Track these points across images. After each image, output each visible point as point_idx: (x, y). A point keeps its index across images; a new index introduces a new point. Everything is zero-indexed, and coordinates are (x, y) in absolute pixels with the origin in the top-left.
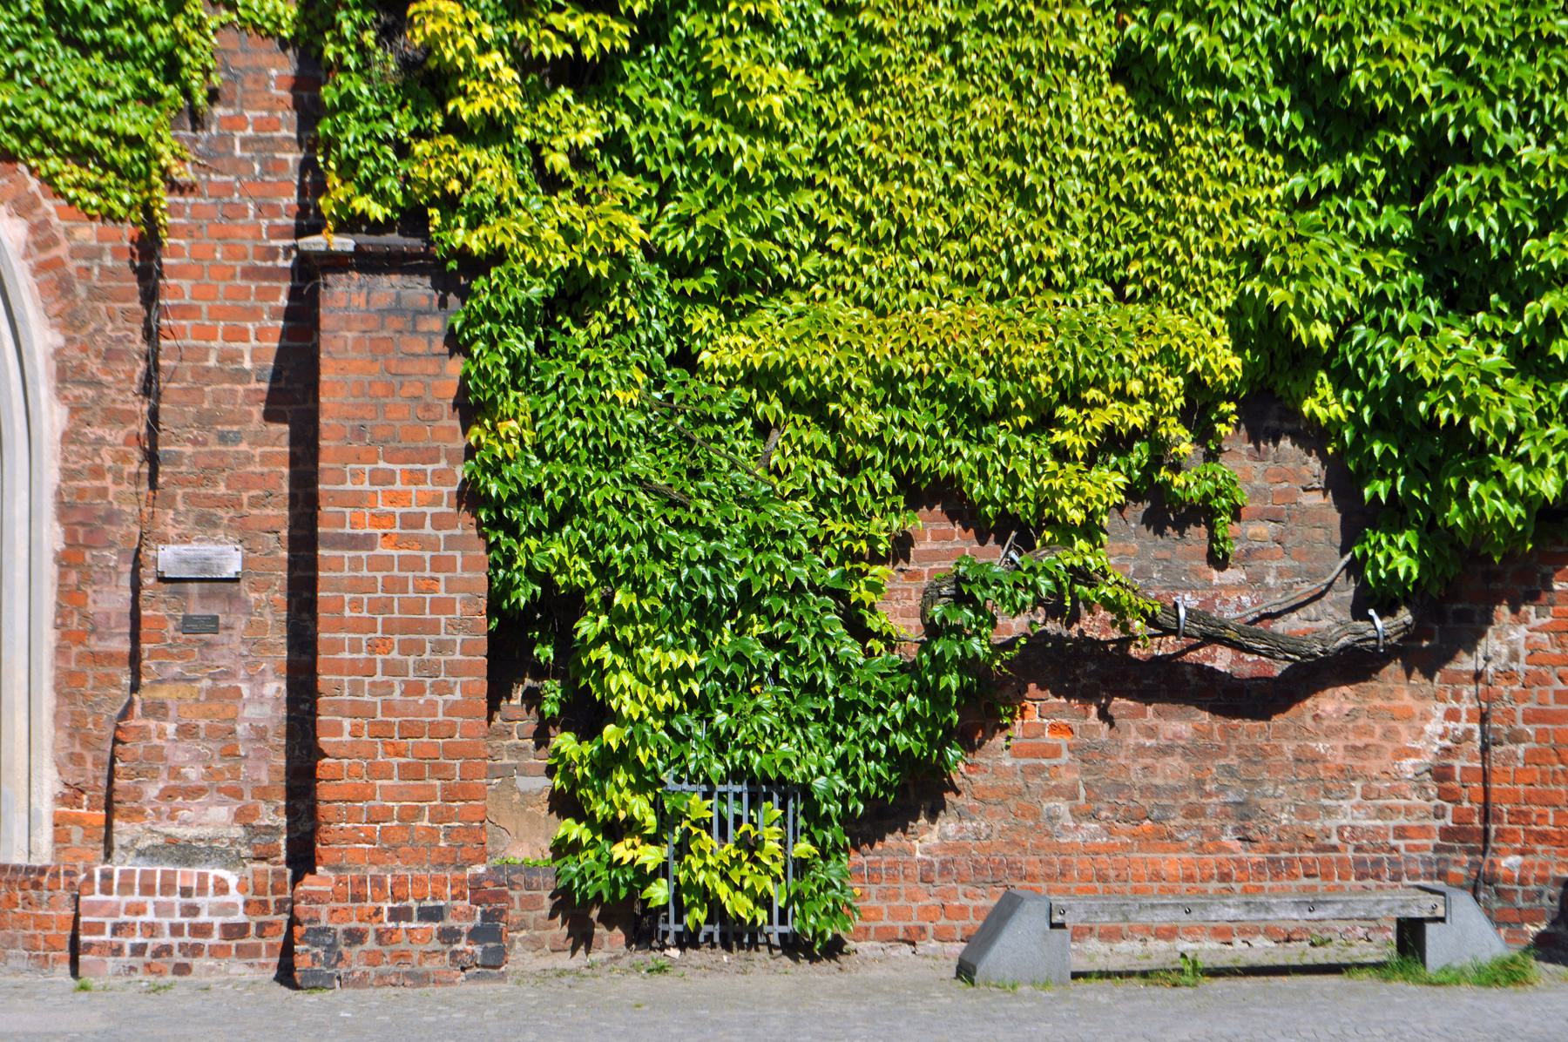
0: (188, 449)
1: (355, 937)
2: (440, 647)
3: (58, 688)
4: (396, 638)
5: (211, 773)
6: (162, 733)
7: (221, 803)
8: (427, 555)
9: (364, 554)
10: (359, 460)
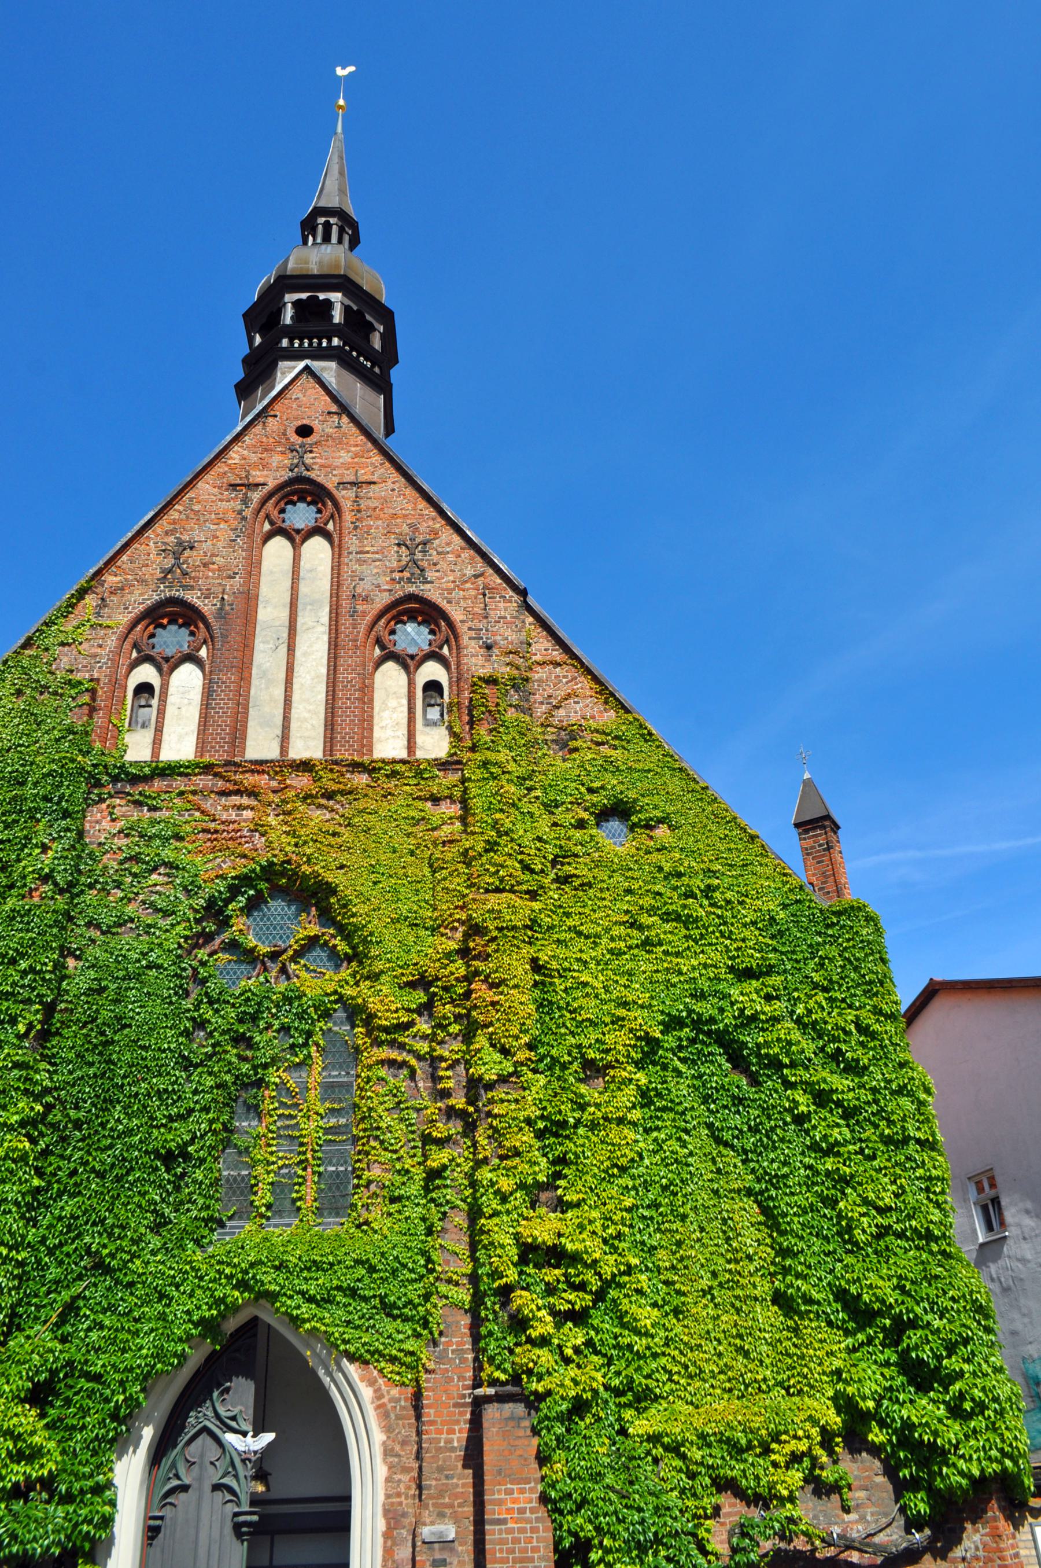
0: (434, 1483)
8: (528, 1526)
9: (503, 1527)
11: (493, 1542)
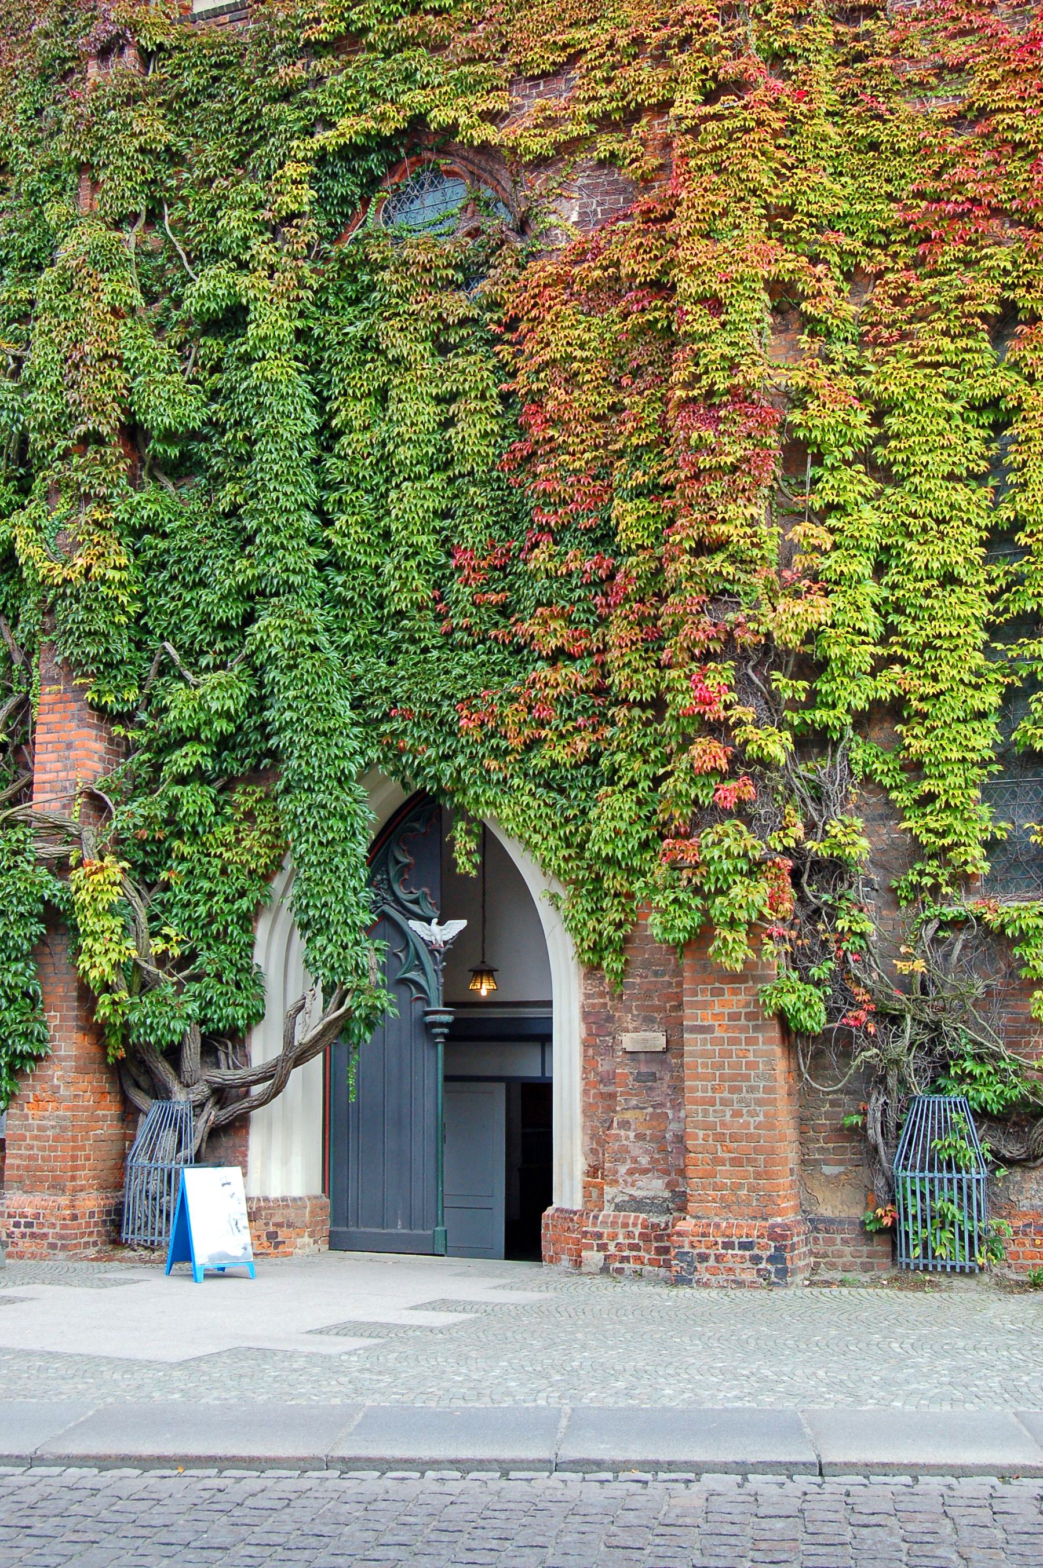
0: (638, 980)
1: (703, 1258)
2: (752, 1090)
3: (584, 1112)
4: (727, 1084)
5: (653, 1161)
6: (627, 1138)
7: (658, 1178)
8: (743, 1036)
9: (708, 1036)
10: (704, 983)
11: (692, 1054)
